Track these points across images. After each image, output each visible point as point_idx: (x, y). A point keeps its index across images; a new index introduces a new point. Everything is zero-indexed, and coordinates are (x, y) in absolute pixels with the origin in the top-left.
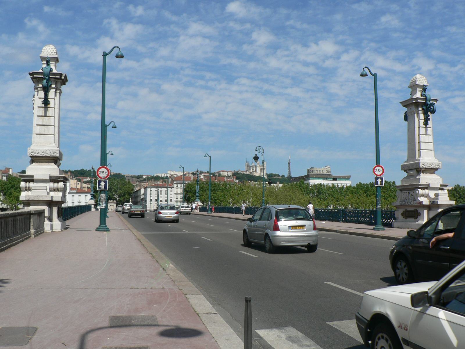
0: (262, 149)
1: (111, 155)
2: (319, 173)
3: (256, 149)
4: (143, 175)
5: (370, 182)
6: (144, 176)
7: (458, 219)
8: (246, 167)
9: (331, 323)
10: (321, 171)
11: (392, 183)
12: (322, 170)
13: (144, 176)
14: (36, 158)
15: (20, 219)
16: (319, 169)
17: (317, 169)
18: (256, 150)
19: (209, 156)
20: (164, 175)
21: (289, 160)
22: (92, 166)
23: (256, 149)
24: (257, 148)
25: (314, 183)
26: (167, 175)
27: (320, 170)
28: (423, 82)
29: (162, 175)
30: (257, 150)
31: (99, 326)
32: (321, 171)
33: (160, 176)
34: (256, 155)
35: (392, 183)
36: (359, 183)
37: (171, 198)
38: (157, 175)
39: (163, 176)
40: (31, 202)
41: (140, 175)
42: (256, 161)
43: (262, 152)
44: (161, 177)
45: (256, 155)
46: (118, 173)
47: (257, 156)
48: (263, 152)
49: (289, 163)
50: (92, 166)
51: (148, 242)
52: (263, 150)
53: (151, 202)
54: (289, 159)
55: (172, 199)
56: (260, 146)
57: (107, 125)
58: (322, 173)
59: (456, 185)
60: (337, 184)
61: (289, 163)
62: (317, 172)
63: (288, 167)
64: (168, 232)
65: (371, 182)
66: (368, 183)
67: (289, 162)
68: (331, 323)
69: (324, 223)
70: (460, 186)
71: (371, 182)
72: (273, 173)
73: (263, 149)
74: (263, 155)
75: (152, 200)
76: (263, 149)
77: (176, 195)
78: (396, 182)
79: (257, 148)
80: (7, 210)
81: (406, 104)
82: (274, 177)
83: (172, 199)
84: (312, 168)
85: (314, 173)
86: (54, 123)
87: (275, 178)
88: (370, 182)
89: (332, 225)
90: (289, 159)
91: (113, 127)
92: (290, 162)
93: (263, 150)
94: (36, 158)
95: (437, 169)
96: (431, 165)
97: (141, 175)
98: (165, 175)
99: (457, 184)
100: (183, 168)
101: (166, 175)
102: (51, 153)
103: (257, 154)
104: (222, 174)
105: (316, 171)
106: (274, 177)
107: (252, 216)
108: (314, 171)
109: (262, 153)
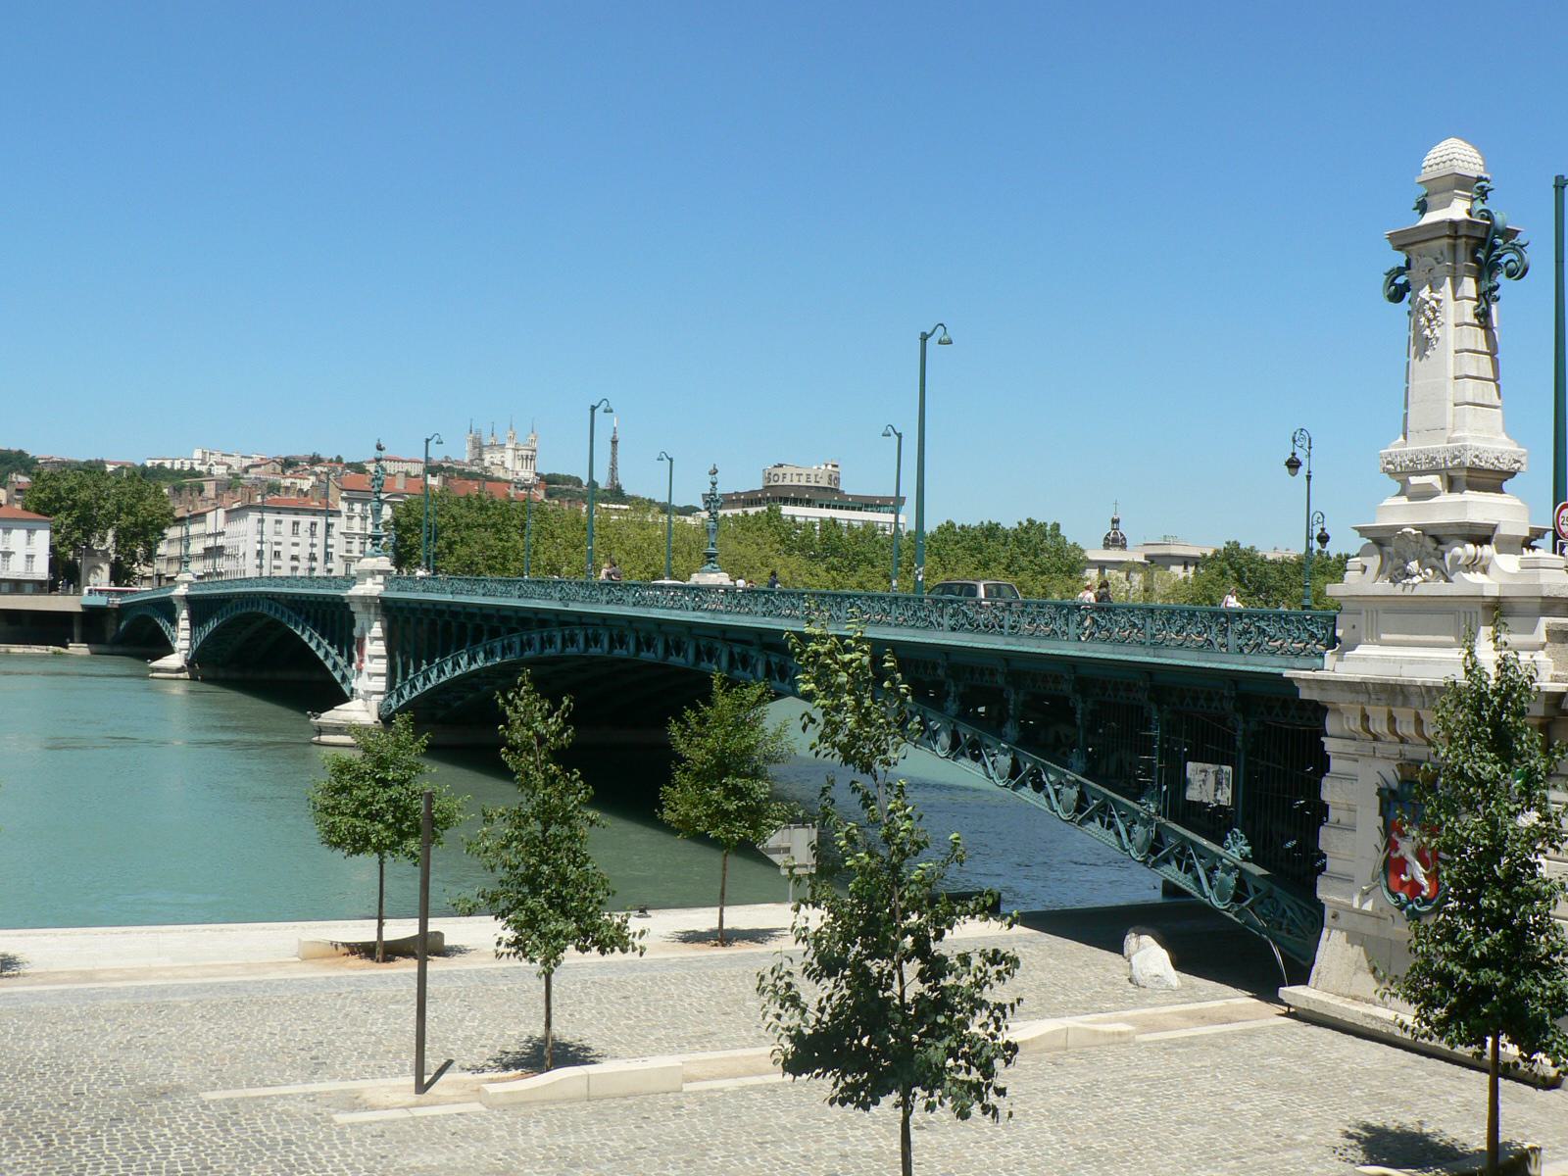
2: (803, 483)
6: (111, 464)
7: (118, 625)
8: (468, 447)
10: (812, 479)
11: (1048, 528)
16: (804, 472)
17: (799, 471)
18: (1294, 441)
20: (182, 463)
25: (806, 517)
28: (1435, 167)
29: (173, 464)
32: (812, 479)
33: (168, 465)
34: (1294, 454)
35: (1048, 528)
38: (157, 462)
39: (177, 466)
41: (93, 459)
44: (172, 468)
45: (1294, 454)
46: (15, 448)
48: (1310, 448)
49: (614, 442)
53: (258, 547)
58: (813, 484)
59: (1228, 543)
61: (614, 442)
63: (609, 456)
65: (986, 523)
66: (975, 523)
67: (614, 437)
70: (1241, 546)
72: (561, 473)
81: (1402, 241)
82: (565, 487)
84: (781, 466)
85: (787, 482)
87: (567, 490)
95: (1512, 474)
96: (1498, 459)
99: (1232, 540)
105: (796, 478)
106: (565, 487)
108: (788, 477)
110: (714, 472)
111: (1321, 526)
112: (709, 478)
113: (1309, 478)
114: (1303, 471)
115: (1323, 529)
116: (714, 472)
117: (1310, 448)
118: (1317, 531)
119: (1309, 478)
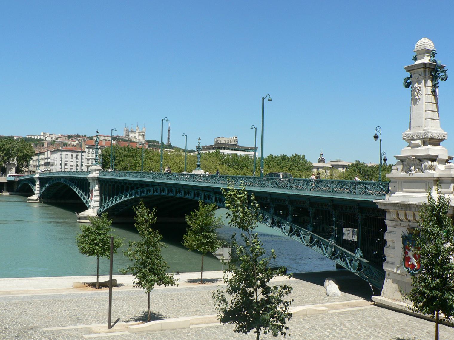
1: (166, 121)
2: (227, 143)
3: (376, 129)
4: (14, 136)
5: (281, 155)
7: (18, 186)
8: (124, 132)
9: (368, 261)
10: (229, 141)
11: (301, 157)
12: (231, 141)
13: (15, 137)
14: (432, 140)
15: (60, 180)
17: (225, 139)
18: (376, 130)
19: (255, 127)
20: (37, 137)
21: (168, 127)
22: (97, 130)
26: (40, 137)
27: (228, 140)
29: (34, 137)
30: (377, 129)
32: (229, 141)
33: (33, 137)
34: (376, 134)
35: (301, 157)
36: (271, 155)
37: (72, 160)
39: (36, 138)
42: (376, 139)
43: (380, 131)
44: (34, 138)
45: (376, 134)
47: (377, 135)
48: (381, 132)
49: (169, 130)
50: (97, 130)
54: (169, 126)
55: (67, 164)
57: (265, 97)
58: (229, 143)
59: (356, 161)
60: (241, 154)
61: (169, 130)
62: (225, 142)
63: (168, 135)
65: (282, 155)
66: (279, 155)
67: (169, 129)
68: (368, 261)
70: (360, 162)
71: (282, 155)
72: (153, 140)
73: (381, 130)
75: (68, 164)
76: (381, 130)
77: (87, 160)
78: (387, 160)
83: (67, 164)
86: (266, 96)
88: (281, 155)
90: (169, 126)
92: (170, 129)
94: (432, 140)
97: (12, 135)
98: (38, 136)
101: (39, 138)
102: (443, 136)
103: (377, 133)
104: (100, 139)
105: (224, 141)
108: (222, 141)
110: (200, 139)
111: (384, 156)
112: (198, 141)
113: (381, 141)
114: (379, 139)
115: (385, 157)
116: (200, 139)
117: (381, 132)
118: (383, 158)
119: (381, 141)
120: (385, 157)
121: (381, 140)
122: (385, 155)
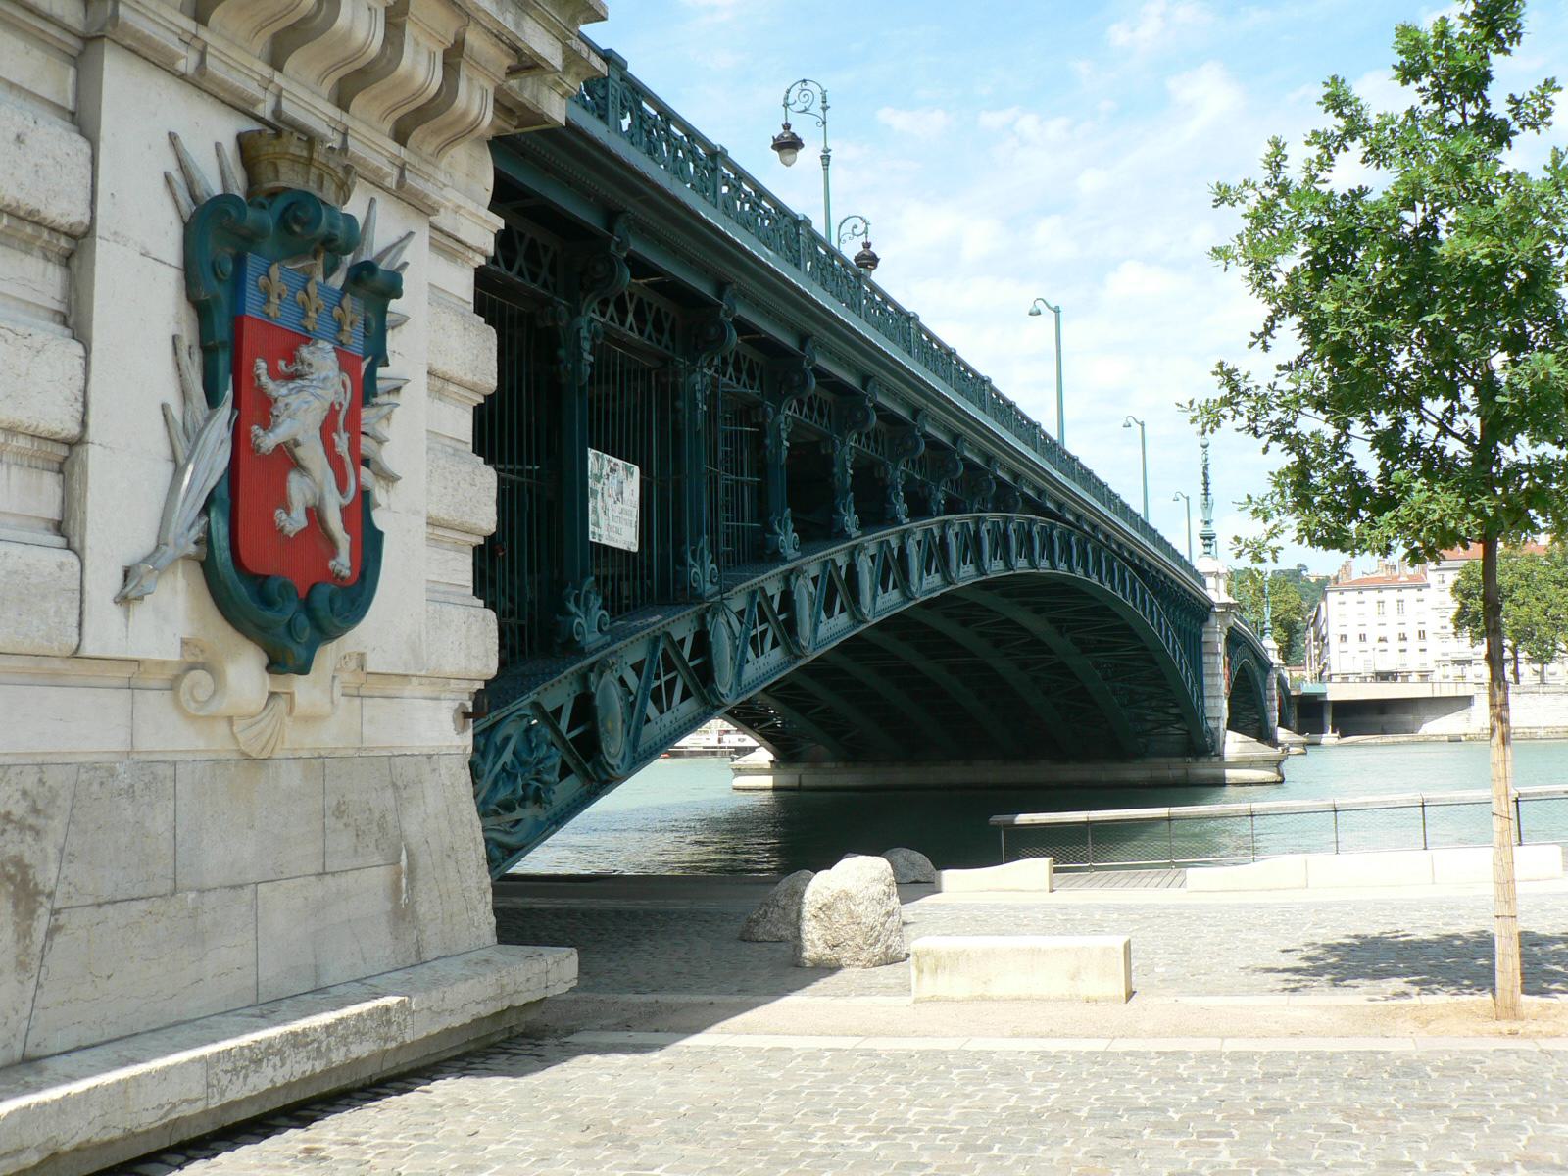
0: (817, 91)
3: (787, 98)
18: (786, 105)
19: (1049, 307)
23: (787, 98)
24: (788, 92)
31: (93, 1042)
34: (787, 127)
40: (804, 564)
42: (789, 158)
45: (787, 127)
48: (825, 109)
51: (546, 689)
52: (824, 97)
56: (804, 81)
64: (672, 661)
69: (244, 590)
74: (824, 123)
79: (788, 92)
80: (1406, 678)
89: (77, 631)
91: (1031, 314)
93: (824, 97)
100: (1142, 425)
107: (1281, 662)
109: (821, 113)
111: (863, 239)
113: (826, 159)
115: (867, 245)
119: (826, 159)
120: (867, 245)
121: (827, 151)
122: (866, 232)
